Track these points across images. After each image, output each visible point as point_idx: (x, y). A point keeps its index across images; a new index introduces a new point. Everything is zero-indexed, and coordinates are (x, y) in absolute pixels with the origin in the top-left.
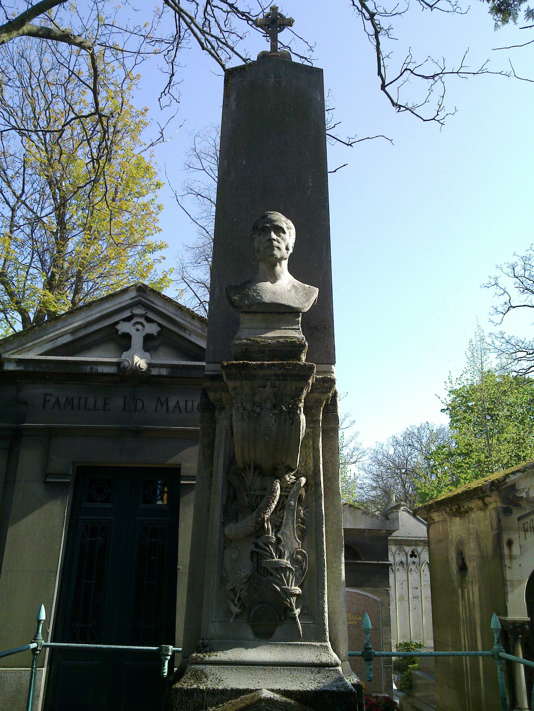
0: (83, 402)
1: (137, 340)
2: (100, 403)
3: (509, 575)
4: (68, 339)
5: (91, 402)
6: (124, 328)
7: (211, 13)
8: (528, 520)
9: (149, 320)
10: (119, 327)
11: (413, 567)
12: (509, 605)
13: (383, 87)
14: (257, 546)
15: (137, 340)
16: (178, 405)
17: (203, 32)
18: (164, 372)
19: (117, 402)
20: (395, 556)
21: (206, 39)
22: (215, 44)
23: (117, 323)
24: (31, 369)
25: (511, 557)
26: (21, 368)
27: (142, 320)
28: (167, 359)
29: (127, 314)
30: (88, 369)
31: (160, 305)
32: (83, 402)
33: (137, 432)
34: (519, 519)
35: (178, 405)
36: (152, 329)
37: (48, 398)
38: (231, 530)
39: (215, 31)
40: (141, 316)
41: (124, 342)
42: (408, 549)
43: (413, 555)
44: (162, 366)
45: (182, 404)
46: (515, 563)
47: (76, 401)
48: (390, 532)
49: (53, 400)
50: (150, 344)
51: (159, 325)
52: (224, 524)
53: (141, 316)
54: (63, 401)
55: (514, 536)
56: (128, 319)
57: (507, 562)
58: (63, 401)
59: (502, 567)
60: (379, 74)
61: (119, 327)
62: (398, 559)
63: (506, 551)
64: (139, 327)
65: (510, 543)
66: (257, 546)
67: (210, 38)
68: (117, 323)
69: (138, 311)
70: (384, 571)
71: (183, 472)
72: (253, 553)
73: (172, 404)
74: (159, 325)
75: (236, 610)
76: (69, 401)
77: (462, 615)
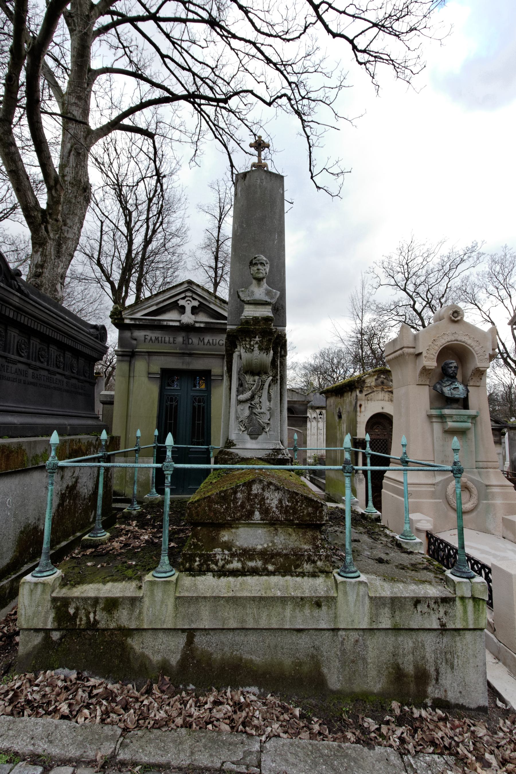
0: (163, 339)
1: (188, 309)
2: (172, 340)
3: (359, 419)
4: (154, 308)
5: (167, 339)
6: (181, 303)
7: (219, 112)
8: (369, 396)
9: (194, 299)
10: (179, 302)
11: (320, 420)
12: (358, 431)
13: (312, 177)
14: (251, 404)
15: (188, 309)
16: (209, 342)
17: (215, 125)
18: (202, 325)
19: (180, 339)
20: (310, 414)
21: (217, 129)
22: (221, 132)
23: (178, 300)
24: (138, 323)
25: (360, 412)
26: (133, 322)
27: (191, 299)
28: (203, 318)
29: (183, 295)
30: (165, 323)
31: (199, 291)
32: (163, 339)
33: (190, 355)
34: (366, 395)
35: (209, 342)
36: (196, 303)
38: (242, 397)
39: (222, 125)
40: (190, 297)
41: (182, 310)
42: (318, 411)
43: (320, 414)
44: (201, 322)
45: (211, 341)
46: (362, 415)
47: (160, 339)
48: (309, 402)
49: (149, 338)
50: (195, 311)
51: (199, 301)
52: (237, 396)
53: (190, 297)
54: (153, 338)
55: (363, 403)
56: (183, 298)
57: (358, 414)
58: (153, 338)
59: (356, 415)
60: (310, 170)
61: (179, 302)
62: (313, 416)
63: (358, 409)
64: (189, 302)
65: (361, 406)
66: (251, 404)
67: (219, 129)
68: (178, 300)
69: (189, 294)
70: (305, 420)
71: (212, 373)
72: (249, 407)
73: (206, 341)
74: (199, 301)
75: (243, 429)
76: (157, 339)
77: (338, 437)
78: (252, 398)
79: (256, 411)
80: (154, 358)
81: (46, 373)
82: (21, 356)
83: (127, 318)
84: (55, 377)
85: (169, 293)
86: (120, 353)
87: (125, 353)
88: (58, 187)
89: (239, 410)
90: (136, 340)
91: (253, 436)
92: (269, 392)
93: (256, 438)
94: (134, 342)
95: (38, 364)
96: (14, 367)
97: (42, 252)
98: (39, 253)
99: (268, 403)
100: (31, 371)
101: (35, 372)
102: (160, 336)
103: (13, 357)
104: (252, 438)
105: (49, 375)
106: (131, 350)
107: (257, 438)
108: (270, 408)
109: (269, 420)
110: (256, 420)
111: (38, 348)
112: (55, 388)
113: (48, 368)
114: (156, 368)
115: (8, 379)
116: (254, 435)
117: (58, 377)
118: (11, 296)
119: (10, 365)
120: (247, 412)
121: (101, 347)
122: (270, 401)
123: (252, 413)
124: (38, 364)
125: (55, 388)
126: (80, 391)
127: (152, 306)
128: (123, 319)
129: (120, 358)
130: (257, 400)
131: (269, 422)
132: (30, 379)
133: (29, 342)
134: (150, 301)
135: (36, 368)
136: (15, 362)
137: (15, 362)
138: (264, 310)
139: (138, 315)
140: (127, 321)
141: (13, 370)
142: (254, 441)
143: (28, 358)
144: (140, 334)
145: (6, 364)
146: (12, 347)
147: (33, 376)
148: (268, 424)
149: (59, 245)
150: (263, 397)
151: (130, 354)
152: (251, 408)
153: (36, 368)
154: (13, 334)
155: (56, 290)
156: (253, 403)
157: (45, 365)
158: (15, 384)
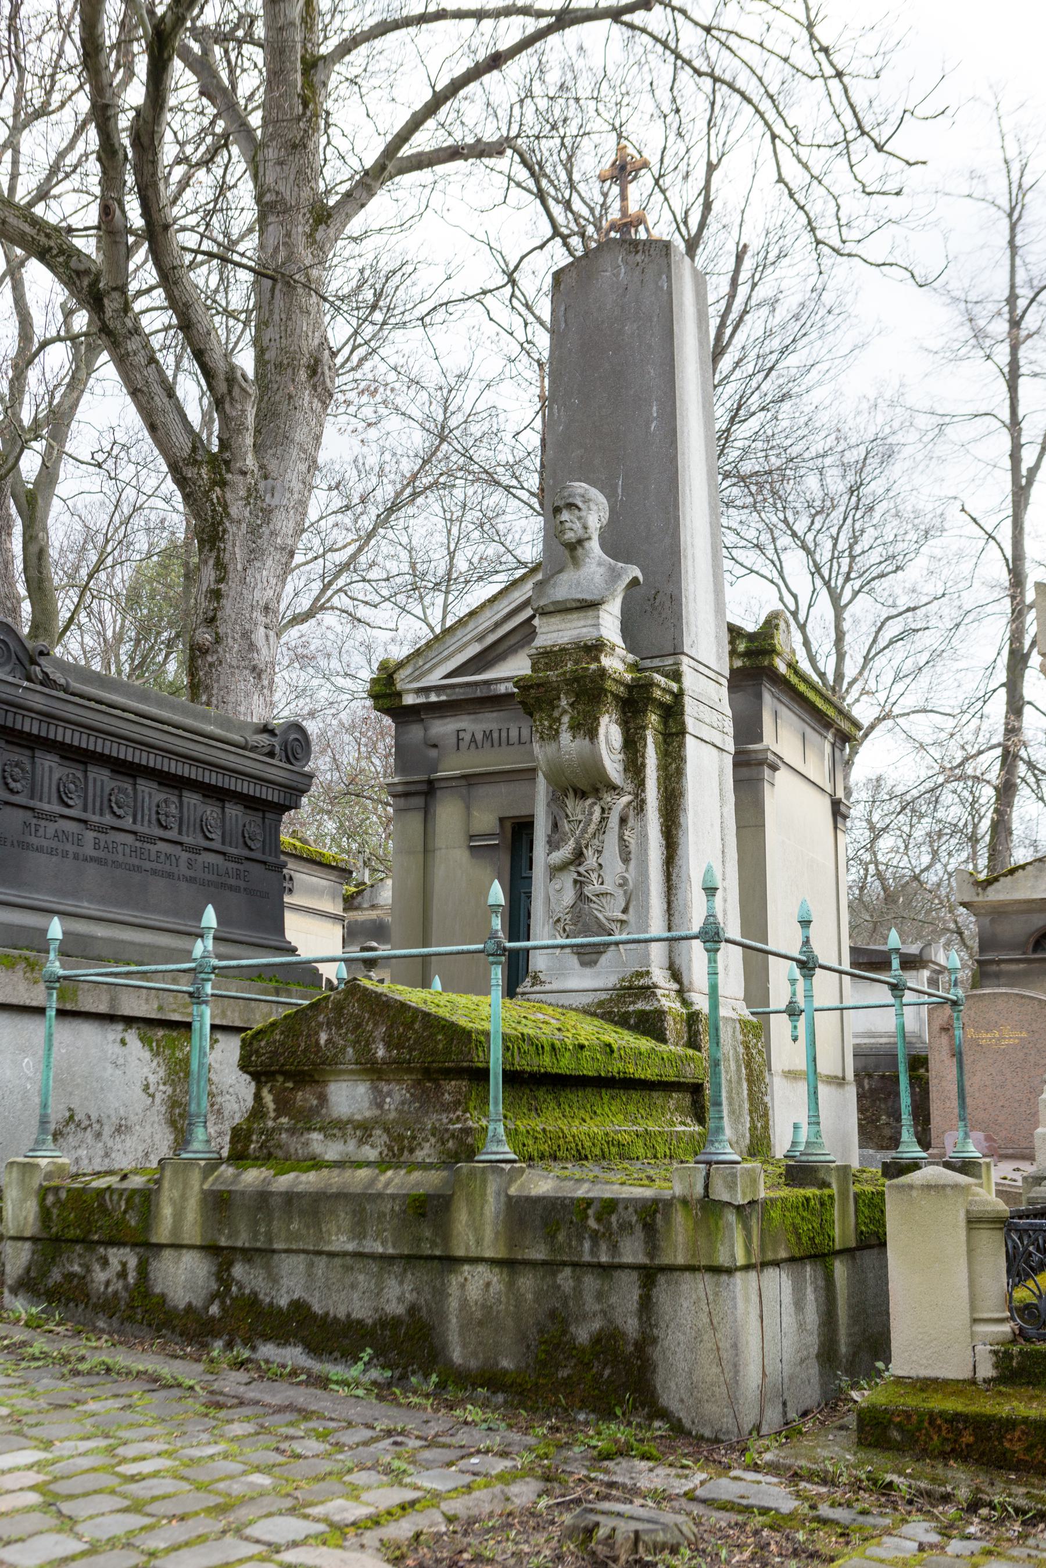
0: (504, 734)
4: (475, 649)
5: (514, 733)
14: (579, 874)
26: (421, 700)
32: (504, 734)
37: (462, 735)
47: (495, 735)
49: (467, 737)
54: (479, 737)
58: (479, 737)
72: (575, 881)
76: (488, 735)
78: (579, 856)
79: (588, 890)
80: (482, 791)
81: (129, 839)
82: (69, 806)
83: (408, 691)
84: (153, 848)
85: (505, 602)
86: (400, 788)
87: (412, 788)
88: (236, 391)
89: (551, 892)
90: (435, 746)
91: (587, 958)
92: (621, 838)
93: (592, 963)
94: (433, 753)
95: (108, 819)
96: (51, 827)
97: (218, 558)
98: (211, 562)
99: (620, 866)
100: (91, 835)
101: (192, 856)
102: (494, 726)
103: (46, 807)
104: (583, 964)
105: (138, 844)
106: (424, 777)
107: (596, 962)
108: (624, 879)
109: (625, 911)
110: (591, 914)
111: (107, 790)
112: (154, 872)
113: (135, 828)
114: (486, 820)
115: (39, 849)
116: (588, 955)
117: (161, 846)
118: (30, 696)
119: (43, 823)
120: (569, 896)
121: (295, 777)
122: (626, 860)
123: (581, 897)
124: (108, 819)
125: (154, 872)
126: (232, 882)
127: (465, 645)
128: (399, 695)
129: (402, 802)
130: (591, 859)
131: (624, 917)
132: (89, 850)
133: (86, 777)
134: (459, 634)
135: (102, 829)
136: (52, 817)
137: (52, 817)
138: (582, 623)
139: (434, 678)
140: (409, 700)
141: (50, 832)
142: (588, 971)
143: (85, 810)
144: (443, 728)
145: (34, 821)
146: (46, 789)
147: (96, 846)
148: (622, 922)
149: (254, 531)
150: (606, 853)
151: (424, 787)
152: (579, 884)
153: (102, 829)
154: (47, 764)
155: (252, 647)
156: (581, 869)
157: (128, 823)
158: (54, 859)
